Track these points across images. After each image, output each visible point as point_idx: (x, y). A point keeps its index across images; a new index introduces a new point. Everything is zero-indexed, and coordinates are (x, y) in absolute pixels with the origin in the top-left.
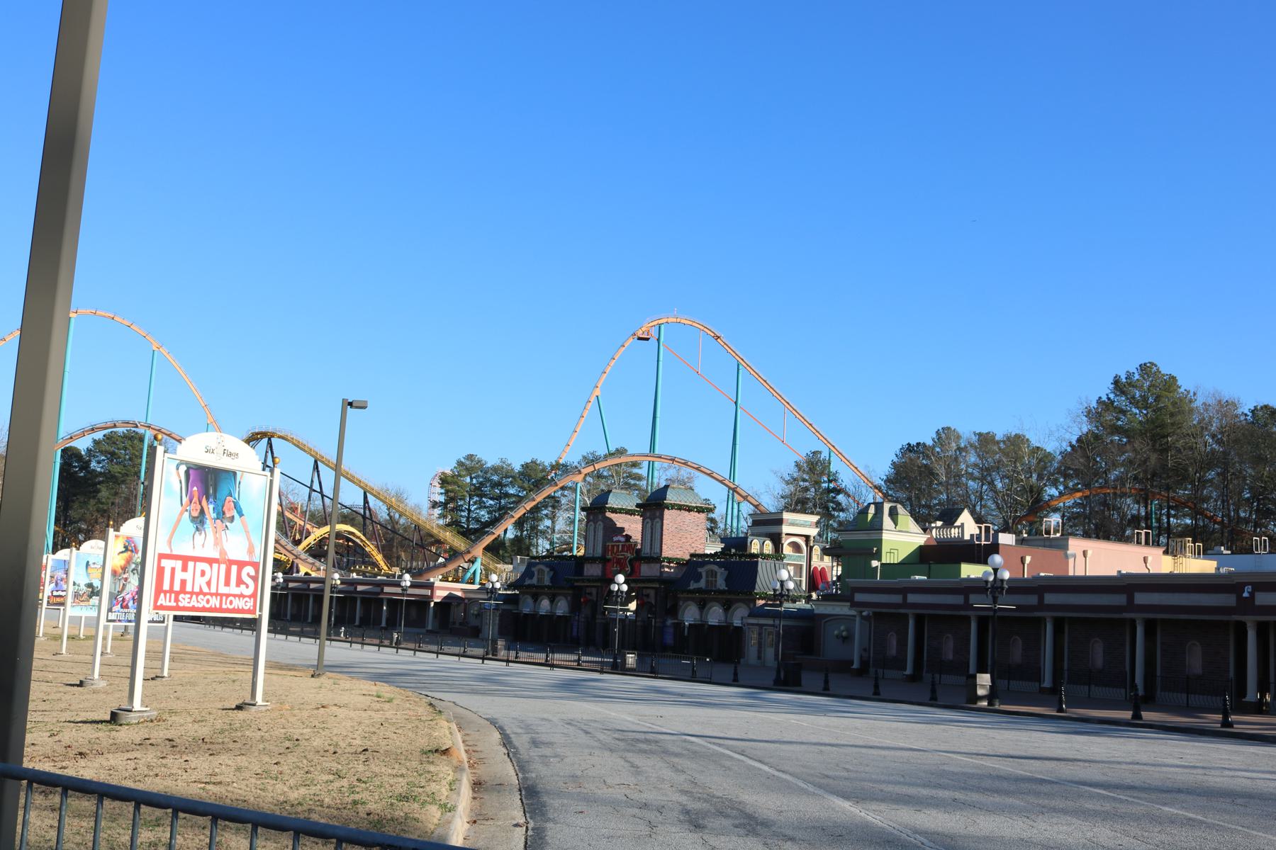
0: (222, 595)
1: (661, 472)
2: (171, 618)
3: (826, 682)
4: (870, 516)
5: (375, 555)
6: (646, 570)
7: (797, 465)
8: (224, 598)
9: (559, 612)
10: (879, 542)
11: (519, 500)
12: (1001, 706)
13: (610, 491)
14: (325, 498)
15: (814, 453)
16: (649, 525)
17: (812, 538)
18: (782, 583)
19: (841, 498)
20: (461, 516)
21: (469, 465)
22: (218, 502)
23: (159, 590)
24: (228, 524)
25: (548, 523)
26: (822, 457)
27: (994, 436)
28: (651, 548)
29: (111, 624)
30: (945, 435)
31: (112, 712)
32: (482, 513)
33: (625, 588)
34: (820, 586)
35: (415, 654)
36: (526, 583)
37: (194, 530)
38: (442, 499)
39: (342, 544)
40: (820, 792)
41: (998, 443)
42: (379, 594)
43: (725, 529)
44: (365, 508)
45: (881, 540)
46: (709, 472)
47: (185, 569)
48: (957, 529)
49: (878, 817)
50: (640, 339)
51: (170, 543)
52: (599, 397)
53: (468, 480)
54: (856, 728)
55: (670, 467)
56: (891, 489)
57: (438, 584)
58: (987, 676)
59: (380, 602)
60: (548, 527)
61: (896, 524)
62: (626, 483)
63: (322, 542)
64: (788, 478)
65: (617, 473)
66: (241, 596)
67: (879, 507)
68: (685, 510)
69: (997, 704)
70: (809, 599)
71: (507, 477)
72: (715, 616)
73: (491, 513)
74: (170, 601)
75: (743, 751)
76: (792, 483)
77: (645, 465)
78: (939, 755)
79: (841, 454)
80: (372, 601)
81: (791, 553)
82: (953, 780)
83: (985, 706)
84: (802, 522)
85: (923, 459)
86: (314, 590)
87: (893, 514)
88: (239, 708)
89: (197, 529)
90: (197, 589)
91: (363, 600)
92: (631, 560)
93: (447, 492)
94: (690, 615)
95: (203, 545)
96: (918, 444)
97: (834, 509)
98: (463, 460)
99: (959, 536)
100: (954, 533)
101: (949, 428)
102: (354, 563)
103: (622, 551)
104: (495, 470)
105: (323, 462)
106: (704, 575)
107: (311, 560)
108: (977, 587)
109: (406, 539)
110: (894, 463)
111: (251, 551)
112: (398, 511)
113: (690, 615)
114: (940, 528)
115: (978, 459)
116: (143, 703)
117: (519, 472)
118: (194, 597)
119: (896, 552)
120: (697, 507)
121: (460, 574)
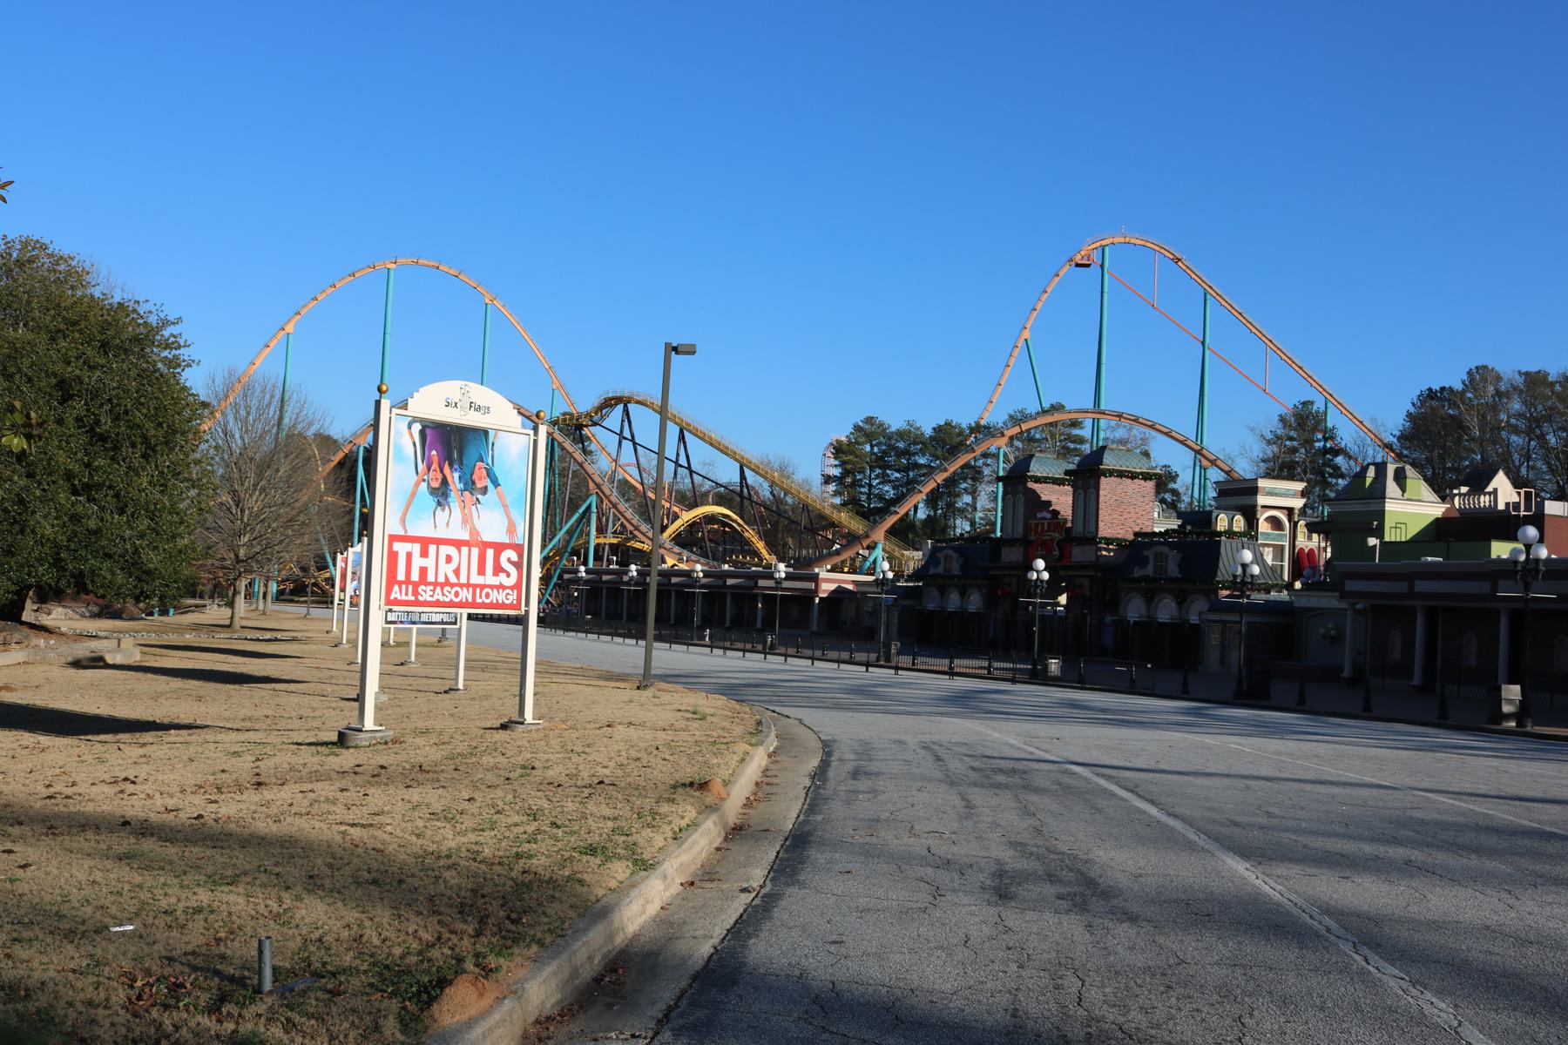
0: (475, 586)
1: (1108, 432)
2: (465, 617)
3: (1302, 694)
4: (1368, 481)
5: (755, 542)
6: (1079, 554)
7: (1282, 419)
8: (478, 590)
9: (972, 608)
10: (1381, 515)
11: (930, 470)
12: (1536, 728)
13: (1032, 456)
14: (694, 475)
15: (1305, 404)
16: (1081, 497)
17: (1297, 512)
18: (1244, 566)
19: (1339, 460)
20: (861, 493)
21: (869, 430)
22: (466, 469)
23: (392, 580)
24: (479, 497)
25: (967, 499)
26: (1315, 408)
27: (1546, 375)
28: (1084, 526)
29: (392, 626)
30: (1480, 376)
31: (339, 732)
32: (886, 488)
33: (1046, 576)
34: (1305, 573)
35: (786, 660)
36: (931, 572)
37: (434, 504)
38: (836, 472)
39: (716, 531)
40: (1211, 846)
41: (1552, 384)
42: (752, 588)
43: (1191, 503)
44: (741, 483)
45: (1383, 512)
46: (1167, 430)
47: (424, 554)
48: (1487, 496)
49: (1280, 887)
50: (1078, 265)
51: (403, 521)
52: (1029, 342)
53: (868, 448)
54: (1317, 756)
55: (1118, 426)
56: (1406, 448)
57: (823, 575)
58: (1518, 688)
59: (755, 598)
60: (968, 504)
61: (1403, 490)
62: (1064, 448)
63: (693, 526)
64: (1269, 436)
65: (1053, 435)
66: (501, 587)
67: (1381, 468)
68: (1127, 477)
69: (1530, 724)
70: (1289, 586)
71: (915, 443)
72: (1166, 611)
73: (898, 489)
74: (407, 594)
75: (1136, 787)
76: (1274, 443)
77: (1088, 423)
78: (1414, 795)
79: (1341, 404)
80: (745, 596)
81: (1270, 531)
82: (1417, 832)
83: (1512, 727)
84: (1283, 491)
85: (1449, 408)
86: (676, 585)
87: (1400, 478)
88: (504, 727)
89: (439, 504)
90: (441, 579)
91: (733, 595)
92: (1059, 541)
93: (843, 464)
94: (1134, 610)
95: (448, 525)
96: (1443, 389)
97: (1331, 475)
98: (861, 424)
99: (1490, 505)
100: (1484, 501)
101: (1485, 367)
102: (732, 552)
103: (1049, 530)
104: (901, 434)
105: (690, 431)
106: (1151, 558)
107: (677, 549)
108: (1508, 569)
109: (793, 522)
110: (1409, 415)
111: (511, 529)
112: (782, 488)
113: (1134, 610)
114: (1464, 495)
115: (1524, 407)
116: (377, 722)
117: (931, 437)
118: (438, 588)
119: (1403, 526)
120: (1142, 473)
121: (857, 564)
